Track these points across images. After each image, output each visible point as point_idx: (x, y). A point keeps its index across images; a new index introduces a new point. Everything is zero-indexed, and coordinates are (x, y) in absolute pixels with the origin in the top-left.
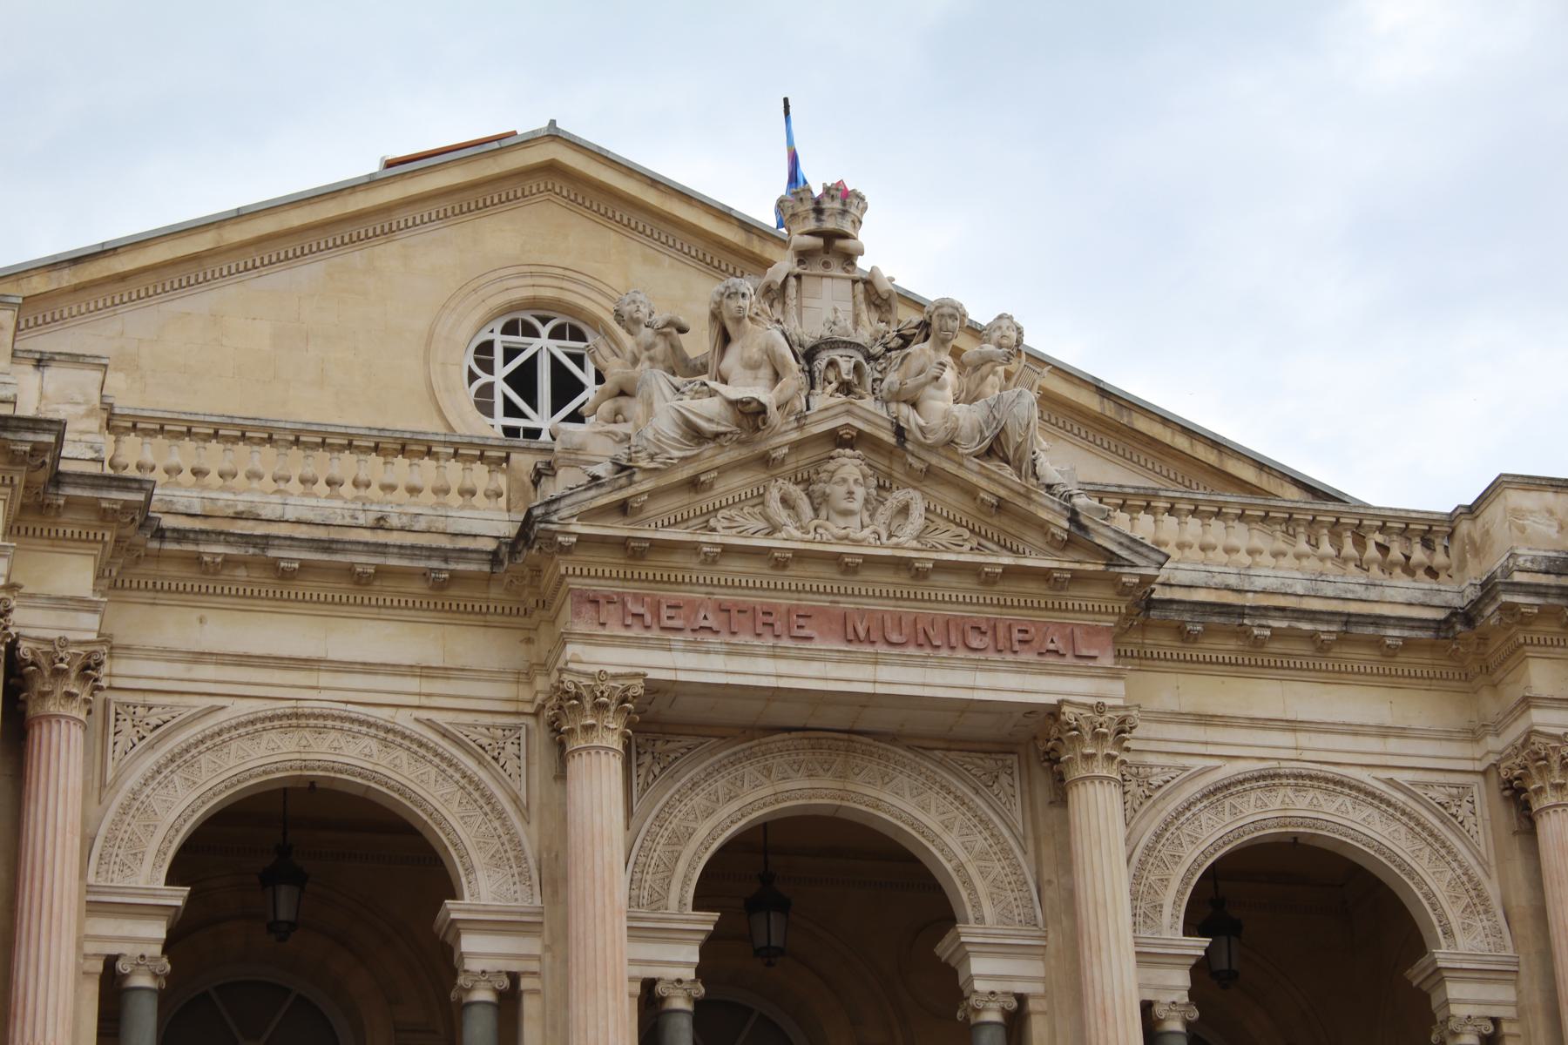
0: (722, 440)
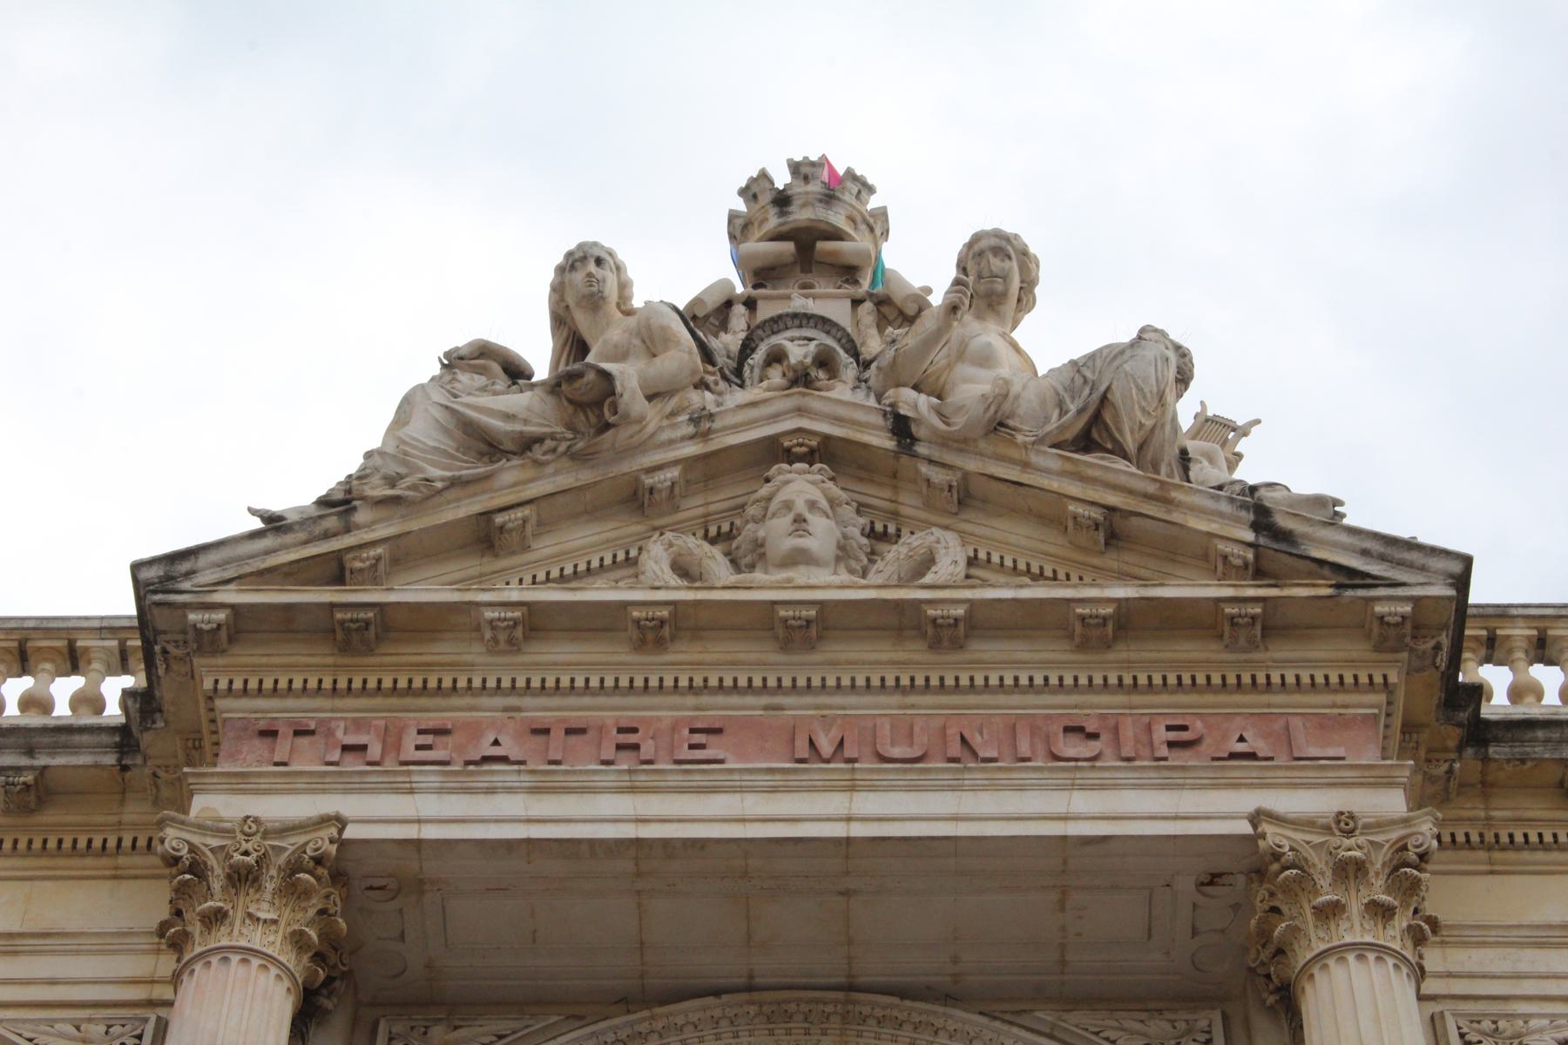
0: (537, 452)
